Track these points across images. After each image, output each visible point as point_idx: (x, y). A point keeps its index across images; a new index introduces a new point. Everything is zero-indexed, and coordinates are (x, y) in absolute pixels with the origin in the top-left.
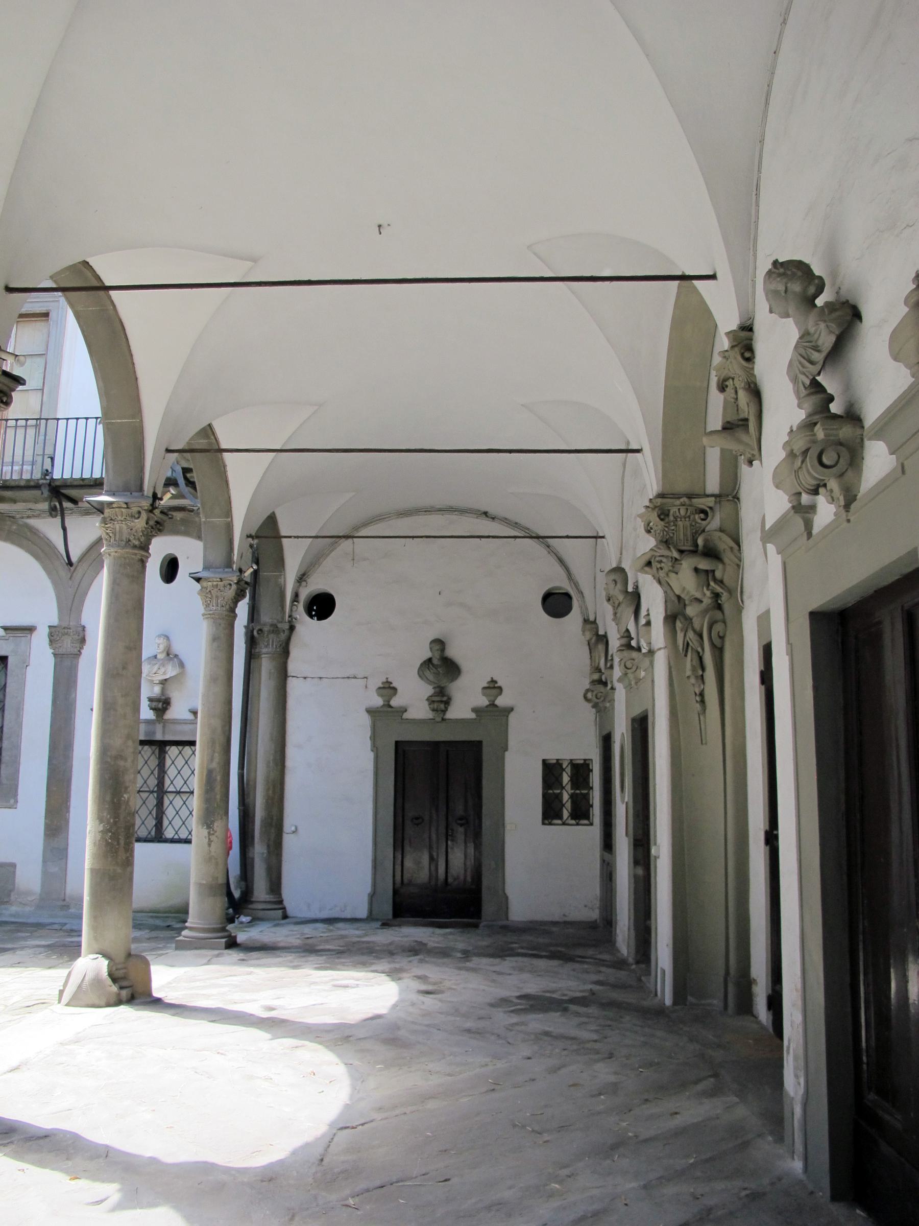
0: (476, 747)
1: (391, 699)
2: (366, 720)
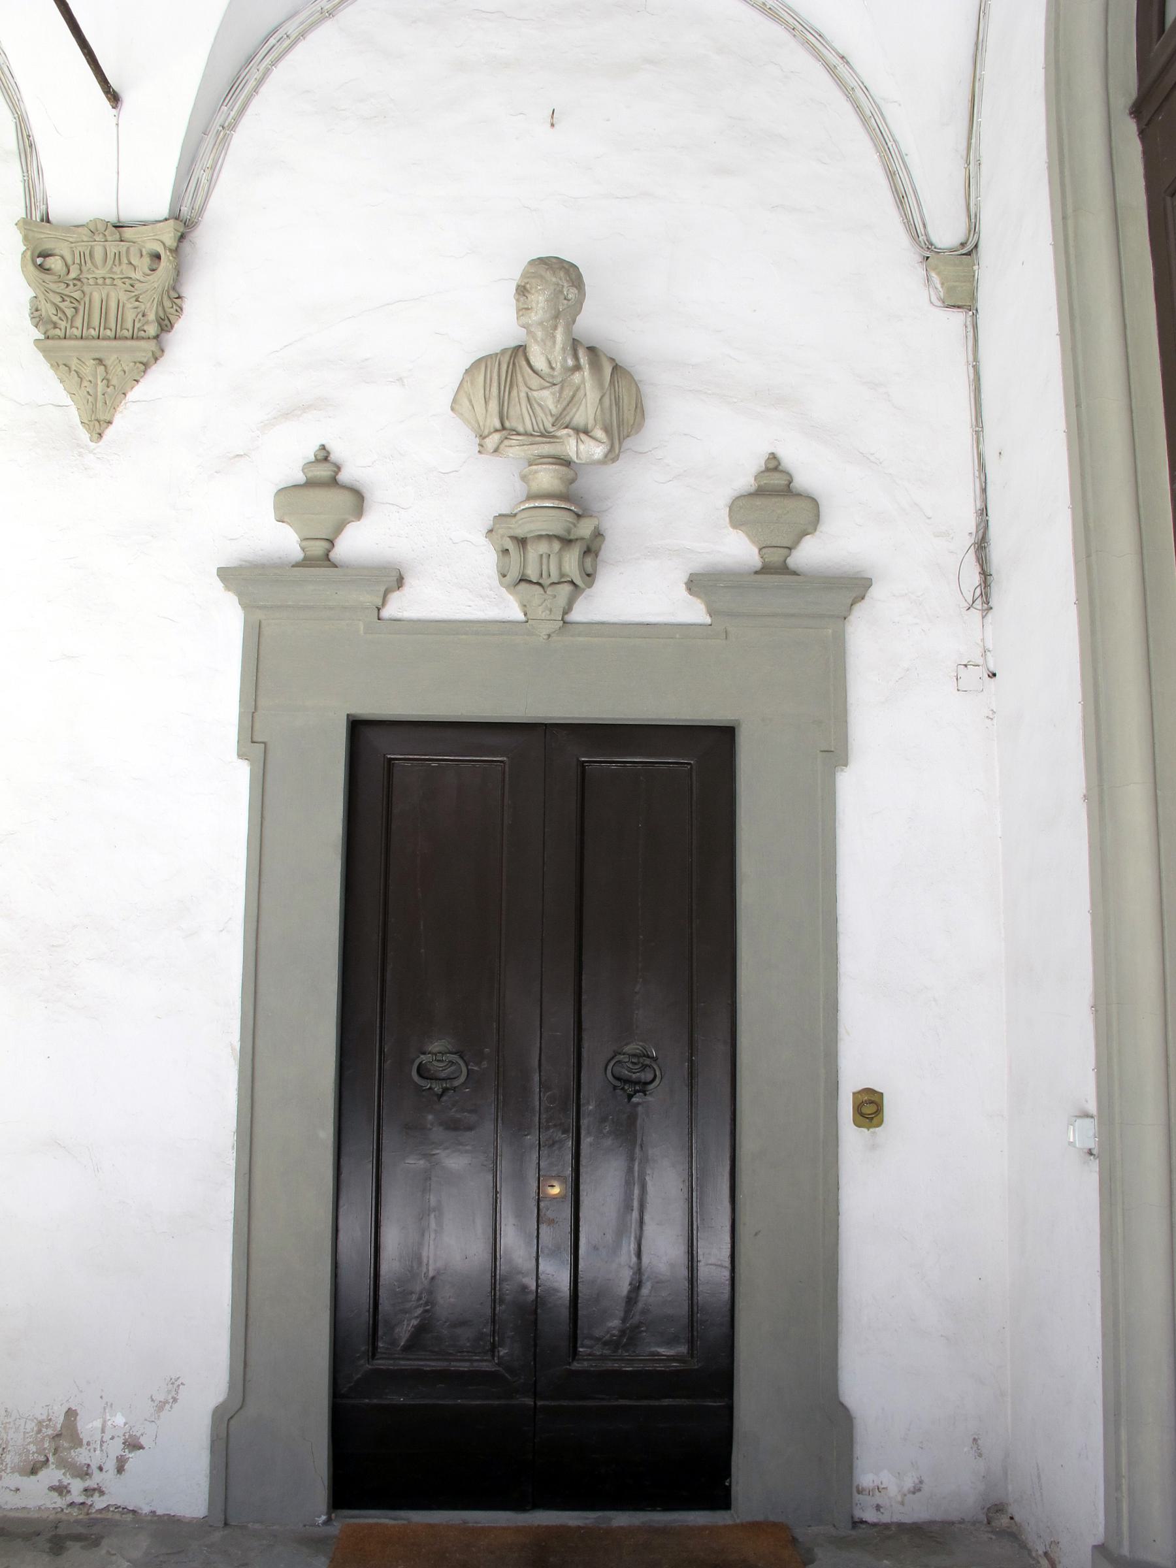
0: (710, 751)
1: (339, 528)
2: (229, 620)
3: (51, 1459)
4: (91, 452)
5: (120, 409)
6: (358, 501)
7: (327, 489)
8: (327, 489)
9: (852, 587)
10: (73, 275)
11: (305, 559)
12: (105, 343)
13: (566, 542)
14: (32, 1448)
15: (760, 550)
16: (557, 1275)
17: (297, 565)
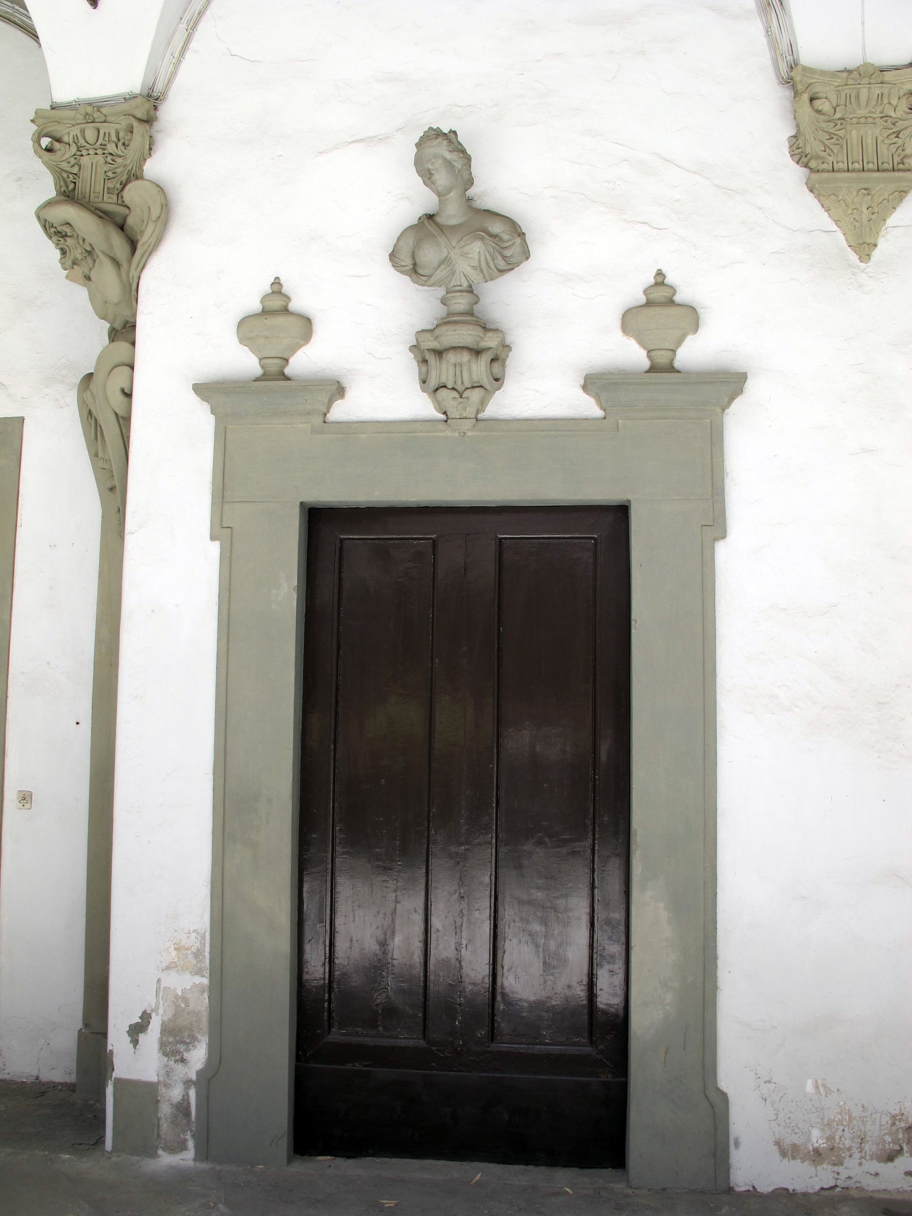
0: (610, 525)
3: (905, 1148)
4: (863, 271)
5: (882, 233)
6: (306, 326)
7: (277, 318)
9: (729, 383)
10: (838, 115)
11: (264, 374)
12: (854, 175)
13: (477, 352)
14: (888, 1138)
15: (260, 360)
16: (477, 967)
17: (257, 380)
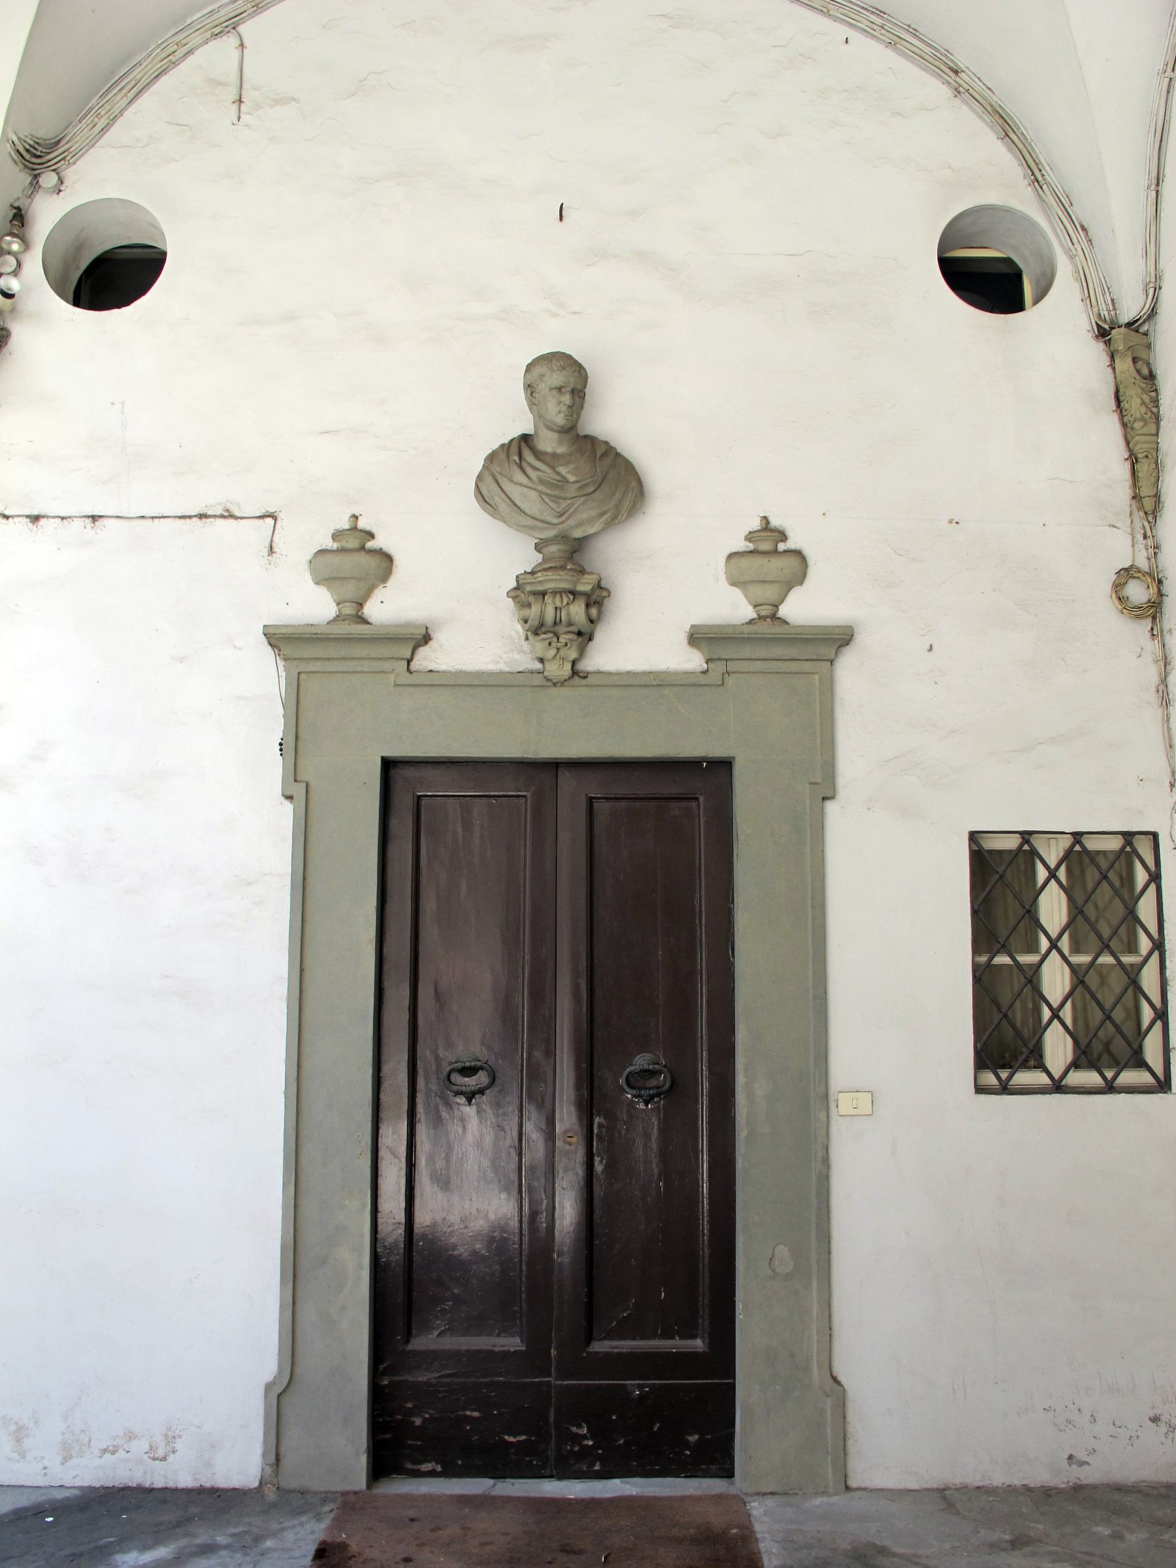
2: (266, 676)
7: (358, 560)
8: (358, 560)
